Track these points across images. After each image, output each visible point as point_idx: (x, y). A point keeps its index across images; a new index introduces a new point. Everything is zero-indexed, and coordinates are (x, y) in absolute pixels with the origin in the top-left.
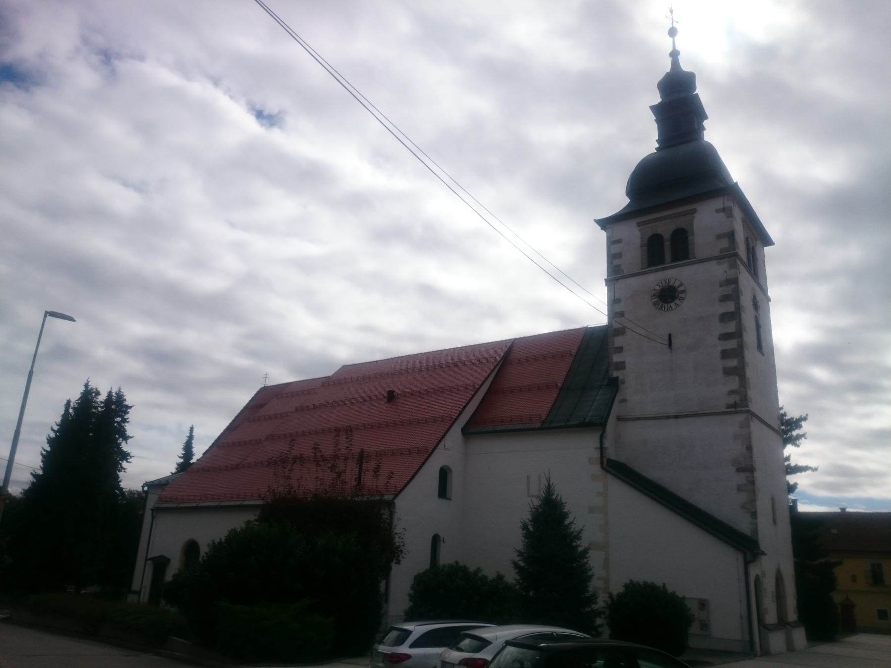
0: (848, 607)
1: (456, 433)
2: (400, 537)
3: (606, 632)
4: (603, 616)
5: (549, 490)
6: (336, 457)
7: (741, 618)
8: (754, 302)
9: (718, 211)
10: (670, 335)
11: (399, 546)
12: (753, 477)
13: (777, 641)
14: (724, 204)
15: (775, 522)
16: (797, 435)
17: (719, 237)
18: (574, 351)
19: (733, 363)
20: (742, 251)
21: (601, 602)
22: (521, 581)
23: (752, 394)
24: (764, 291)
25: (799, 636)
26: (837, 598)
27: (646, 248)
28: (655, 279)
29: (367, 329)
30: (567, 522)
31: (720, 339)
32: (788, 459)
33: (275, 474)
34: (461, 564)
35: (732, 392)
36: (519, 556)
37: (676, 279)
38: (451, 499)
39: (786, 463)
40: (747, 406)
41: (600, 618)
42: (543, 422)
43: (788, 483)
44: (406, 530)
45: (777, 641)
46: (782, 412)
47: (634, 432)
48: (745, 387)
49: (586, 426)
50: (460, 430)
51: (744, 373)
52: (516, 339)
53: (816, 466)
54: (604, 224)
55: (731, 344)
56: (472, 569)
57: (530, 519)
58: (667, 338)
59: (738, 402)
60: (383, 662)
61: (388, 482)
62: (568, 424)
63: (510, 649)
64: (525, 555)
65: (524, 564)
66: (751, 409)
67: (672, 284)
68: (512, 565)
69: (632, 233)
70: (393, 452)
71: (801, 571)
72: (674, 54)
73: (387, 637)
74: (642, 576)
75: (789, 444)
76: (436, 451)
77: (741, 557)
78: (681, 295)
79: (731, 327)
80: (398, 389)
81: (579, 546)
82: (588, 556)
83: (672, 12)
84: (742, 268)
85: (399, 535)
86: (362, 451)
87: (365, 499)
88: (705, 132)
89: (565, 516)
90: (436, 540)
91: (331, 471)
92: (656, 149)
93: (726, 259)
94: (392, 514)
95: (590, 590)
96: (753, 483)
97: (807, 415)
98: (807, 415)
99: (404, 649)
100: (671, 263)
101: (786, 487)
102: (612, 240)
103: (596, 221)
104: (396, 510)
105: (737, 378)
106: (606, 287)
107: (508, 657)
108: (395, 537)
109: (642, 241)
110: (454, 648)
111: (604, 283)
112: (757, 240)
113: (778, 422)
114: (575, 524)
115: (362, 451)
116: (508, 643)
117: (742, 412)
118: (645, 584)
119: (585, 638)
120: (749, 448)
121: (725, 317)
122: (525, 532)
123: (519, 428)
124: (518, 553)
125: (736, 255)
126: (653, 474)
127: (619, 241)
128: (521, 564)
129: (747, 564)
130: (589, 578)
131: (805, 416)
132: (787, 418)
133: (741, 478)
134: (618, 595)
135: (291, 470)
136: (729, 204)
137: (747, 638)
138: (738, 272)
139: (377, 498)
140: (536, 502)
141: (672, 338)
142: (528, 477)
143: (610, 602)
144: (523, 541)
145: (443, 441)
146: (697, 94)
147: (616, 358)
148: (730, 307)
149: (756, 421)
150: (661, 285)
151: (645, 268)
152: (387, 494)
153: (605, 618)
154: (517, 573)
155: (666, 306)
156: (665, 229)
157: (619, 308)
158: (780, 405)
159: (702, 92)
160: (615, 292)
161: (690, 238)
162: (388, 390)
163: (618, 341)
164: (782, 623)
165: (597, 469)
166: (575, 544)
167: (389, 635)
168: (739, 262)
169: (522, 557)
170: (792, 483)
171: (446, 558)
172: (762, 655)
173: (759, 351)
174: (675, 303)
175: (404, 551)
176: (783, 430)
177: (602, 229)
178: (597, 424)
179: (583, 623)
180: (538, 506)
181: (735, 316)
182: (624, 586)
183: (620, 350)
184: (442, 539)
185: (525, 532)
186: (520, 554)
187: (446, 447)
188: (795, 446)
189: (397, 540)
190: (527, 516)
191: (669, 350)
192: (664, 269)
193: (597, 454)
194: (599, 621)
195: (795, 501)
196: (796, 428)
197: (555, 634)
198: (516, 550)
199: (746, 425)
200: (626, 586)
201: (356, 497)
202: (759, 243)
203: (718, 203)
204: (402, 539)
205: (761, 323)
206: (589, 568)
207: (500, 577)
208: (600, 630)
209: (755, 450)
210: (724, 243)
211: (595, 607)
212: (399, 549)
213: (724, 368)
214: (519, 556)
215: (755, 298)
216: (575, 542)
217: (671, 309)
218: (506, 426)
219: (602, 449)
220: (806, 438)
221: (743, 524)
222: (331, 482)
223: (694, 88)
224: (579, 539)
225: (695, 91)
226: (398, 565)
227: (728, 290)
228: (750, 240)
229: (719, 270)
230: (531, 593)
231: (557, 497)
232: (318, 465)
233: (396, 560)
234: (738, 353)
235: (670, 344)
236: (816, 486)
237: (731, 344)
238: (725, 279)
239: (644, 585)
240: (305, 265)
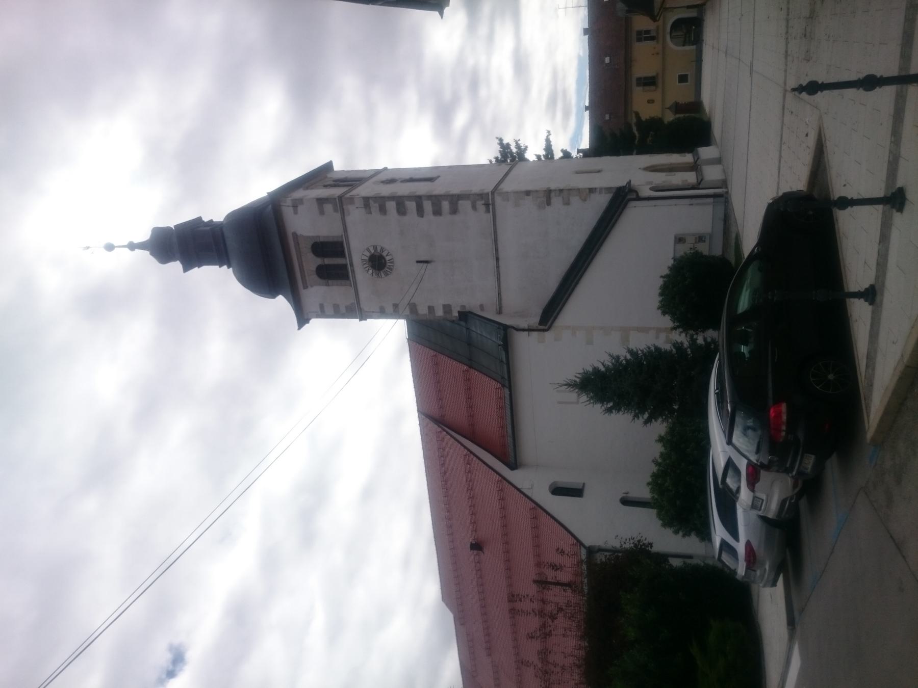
0: (677, 108)
1: (517, 477)
2: (625, 543)
3: (711, 334)
4: (695, 337)
5: (571, 385)
6: (541, 613)
7: (692, 205)
8: (387, 183)
9: (296, 212)
10: (418, 262)
11: (633, 543)
12: (555, 190)
13: (712, 173)
14: (288, 206)
15: (599, 171)
16: (516, 148)
17: (322, 212)
18: (432, 353)
19: (446, 205)
20: (337, 192)
21: (681, 338)
22: (664, 417)
23: (476, 189)
24: (377, 172)
25: (706, 152)
26: (669, 117)
27: (330, 281)
28: (361, 273)
29: (406, 562)
30: (603, 369)
31: (422, 216)
32: (539, 157)
33: (559, 683)
34: (650, 480)
35: (474, 207)
36: (638, 418)
37: (363, 254)
38: (584, 484)
39: (543, 159)
40: (488, 194)
41: (697, 339)
42: (503, 386)
43: (561, 158)
44: (617, 536)
45: (712, 173)
46: (494, 161)
47: (513, 298)
48: (470, 194)
49: (506, 345)
50: (512, 471)
51: (455, 195)
52: (418, 411)
53: (546, 131)
54: (302, 320)
55: (428, 206)
56: (655, 469)
57: (601, 405)
58: (419, 264)
60: (755, 571)
61: (567, 555)
62: (504, 360)
63: (735, 440)
64: (637, 411)
65: (646, 413)
66: (491, 190)
67: (367, 258)
68: (648, 425)
69: (314, 293)
70: (535, 537)
71: (644, 149)
72: (132, 246)
73: (727, 563)
74: (654, 299)
75: (524, 156)
76: (534, 498)
77: (632, 204)
78: (379, 251)
79: (411, 206)
80: (469, 539)
81: (625, 357)
82: (635, 350)
84: (354, 192)
85: (623, 543)
86: (535, 582)
87: (586, 581)
88: (214, 220)
89: (596, 371)
90: (626, 502)
91: (556, 618)
92: (229, 268)
93: (344, 207)
94: (600, 550)
95: (670, 349)
96: (561, 191)
97: (497, 138)
98: (497, 138)
99: (741, 548)
100: (346, 258)
101: (566, 160)
102: (320, 313)
103: (299, 329)
104: (597, 545)
105: (460, 202)
106: (368, 320)
107: (741, 440)
108: (625, 548)
109: (323, 285)
110: (738, 495)
111: (364, 322)
112: (326, 177)
113: (503, 165)
114: (604, 361)
115: (535, 582)
116: (730, 442)
117: (493, 199)
118: (661, 294)
119: (719, 360)
120: (528, 193)
121: (401, 210)
122: (614, 411)
123: (509, 410)
124: (636, 419)
125: (340, 198)
126: (553, 284)
127: (322, 307)
128: (646, 416)
129: (639, 198)
130: (657, 349)
131: (498, 140)
132: (500, 157)
133: (556, 201)
134: (674, 321)
135: (555, 665)
136: (289, 202)
137: (711, 200)
138: (358, 196)
139: (584, 567)
140: (584, 398)
142: (560, 403)
143: (681, 330)
144: (624, 414)
145: (523, 490)
146: (175, 226)
147: (440, 313)
148: (391, 206)
149: (502, 186)
150: (367, 268)
151: (351, 283)
152: (581, 556)
153: (697, 334)
154: (656, 421)
156: (312, 262)
157: (390, 309)
158: (488, 162)
159: (172, 222)
160: (373, 312)
161: (322, 240)
162: (469, 550)
163: (423, 310)
164: (695, 167)
166: (624, 362)
167: (725, 561)
168: (348, 195)
169: (640, 415)
170: (561, 155)
171: (645, 493)
172: (727, 188)
173: (435, 180)
174: (387, 256)
175: (639, 538)
176: (511, 161)
177: (308, 322)
178: (505, 333)
179: (705, 355)
180: (587, 397)
181: (400, 202)
183: (431, 309)
184: (625, 495)
185: (614, 411)
186: (636, 416)
188: (527, 150)
189: (627, 546)
190: (598, 408)
192: (352, 265)
193: (535, 335)
194: (700, 341)
195: (579, 151)
196: (510, 148)
197: (716, 391)
198: (632, 420)
199: (506, 196)
200: (664, 313)
201: (583, 591)
202: (329, 175)
203: (287, 211)
204: (626, 540)
205: (408, 177)
206: (647, 349)
207: (661, 439)
208: (709, 340)
209: (530, 188)
210: (328, 208)
211: (686, 344)
212: (637, 543)
213: (450, 214)
214: (638, 418)
215: (383, 182)
216: (622, 361)
217: (392, 260)
218: (507, 418)
219: (530, 330)
220: (519, 140)
221: (603, 200)
222: (567, 619)
223: (169, 229)
224: (618, 357)
225: (172, 228)
226: (653, 545)
227: (375, 206)
228: (326, 184)
229: (355, 214)
230: (676, 407)
231: (578, 378)
232: (550, 634)
233: (648, 547)
234: (436, 200)
235: (427, 262)
236: (565, 127)
237: (428, 206)
238: (364, 209)
239: (662, 296)
240: (335, 629)
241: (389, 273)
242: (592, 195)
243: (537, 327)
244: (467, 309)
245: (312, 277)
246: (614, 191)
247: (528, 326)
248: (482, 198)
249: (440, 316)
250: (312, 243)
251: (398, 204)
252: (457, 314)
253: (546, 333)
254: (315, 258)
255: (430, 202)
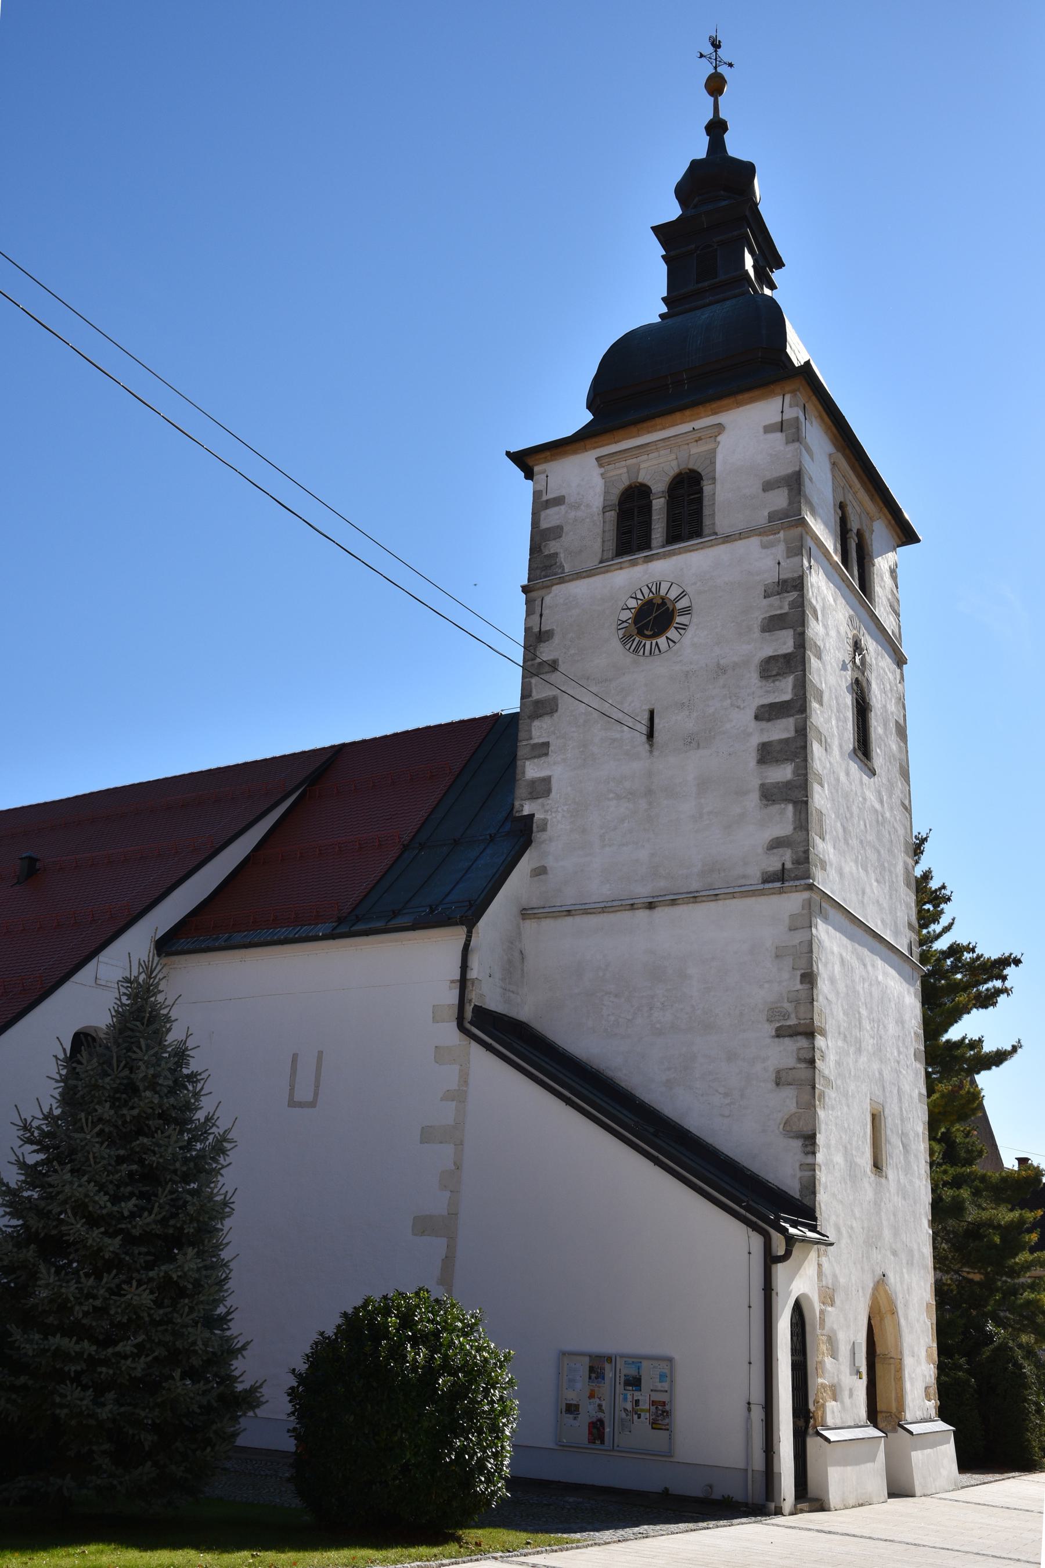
10: (652, 713)
17: (768, 486)
31: (757, 718)
35: (776, 844)
48: (807, 831)
58: (646, 716)
59: (789, 865)
67: (663, 592)
83: (716, 45)
100: (663, 546)
105: (790, 808)
120: (809, 978)
141: (656, 721)
150: (640, 596)
155: (648, 644)
165: (449, 1034)
174: (667, 638)
182: (225, 1204)
187: (99, 982)
191: (647, 746)
199: (803, 923)
213: (762, 785)
227: (782, 605)
235: (650, 735)
237: (781, 730)
241: (628, 647)
242: (797, 1144)
243: (470, 1001)
244: (537, 836)
245: (622, 476)
246: (806, 1201)
247: (473, 981)
248: (797, 862)
249: (524, 773)
250: (699, 470)
251: (787, 658)
252: (526, 811)
253: (455, 1024)
254: (667, 480)
255: (790, 733)
